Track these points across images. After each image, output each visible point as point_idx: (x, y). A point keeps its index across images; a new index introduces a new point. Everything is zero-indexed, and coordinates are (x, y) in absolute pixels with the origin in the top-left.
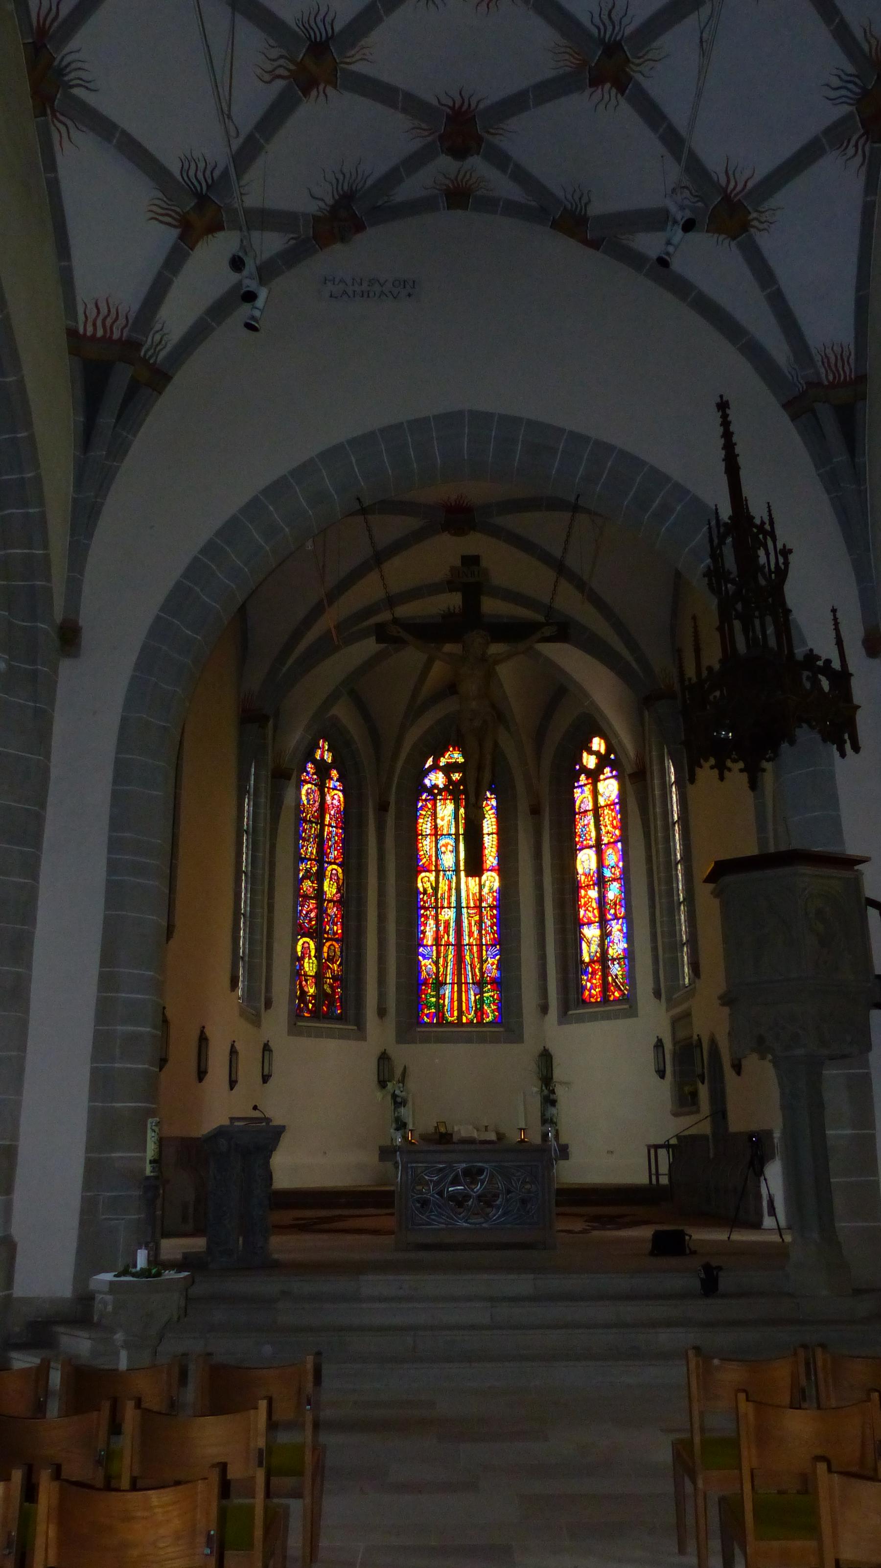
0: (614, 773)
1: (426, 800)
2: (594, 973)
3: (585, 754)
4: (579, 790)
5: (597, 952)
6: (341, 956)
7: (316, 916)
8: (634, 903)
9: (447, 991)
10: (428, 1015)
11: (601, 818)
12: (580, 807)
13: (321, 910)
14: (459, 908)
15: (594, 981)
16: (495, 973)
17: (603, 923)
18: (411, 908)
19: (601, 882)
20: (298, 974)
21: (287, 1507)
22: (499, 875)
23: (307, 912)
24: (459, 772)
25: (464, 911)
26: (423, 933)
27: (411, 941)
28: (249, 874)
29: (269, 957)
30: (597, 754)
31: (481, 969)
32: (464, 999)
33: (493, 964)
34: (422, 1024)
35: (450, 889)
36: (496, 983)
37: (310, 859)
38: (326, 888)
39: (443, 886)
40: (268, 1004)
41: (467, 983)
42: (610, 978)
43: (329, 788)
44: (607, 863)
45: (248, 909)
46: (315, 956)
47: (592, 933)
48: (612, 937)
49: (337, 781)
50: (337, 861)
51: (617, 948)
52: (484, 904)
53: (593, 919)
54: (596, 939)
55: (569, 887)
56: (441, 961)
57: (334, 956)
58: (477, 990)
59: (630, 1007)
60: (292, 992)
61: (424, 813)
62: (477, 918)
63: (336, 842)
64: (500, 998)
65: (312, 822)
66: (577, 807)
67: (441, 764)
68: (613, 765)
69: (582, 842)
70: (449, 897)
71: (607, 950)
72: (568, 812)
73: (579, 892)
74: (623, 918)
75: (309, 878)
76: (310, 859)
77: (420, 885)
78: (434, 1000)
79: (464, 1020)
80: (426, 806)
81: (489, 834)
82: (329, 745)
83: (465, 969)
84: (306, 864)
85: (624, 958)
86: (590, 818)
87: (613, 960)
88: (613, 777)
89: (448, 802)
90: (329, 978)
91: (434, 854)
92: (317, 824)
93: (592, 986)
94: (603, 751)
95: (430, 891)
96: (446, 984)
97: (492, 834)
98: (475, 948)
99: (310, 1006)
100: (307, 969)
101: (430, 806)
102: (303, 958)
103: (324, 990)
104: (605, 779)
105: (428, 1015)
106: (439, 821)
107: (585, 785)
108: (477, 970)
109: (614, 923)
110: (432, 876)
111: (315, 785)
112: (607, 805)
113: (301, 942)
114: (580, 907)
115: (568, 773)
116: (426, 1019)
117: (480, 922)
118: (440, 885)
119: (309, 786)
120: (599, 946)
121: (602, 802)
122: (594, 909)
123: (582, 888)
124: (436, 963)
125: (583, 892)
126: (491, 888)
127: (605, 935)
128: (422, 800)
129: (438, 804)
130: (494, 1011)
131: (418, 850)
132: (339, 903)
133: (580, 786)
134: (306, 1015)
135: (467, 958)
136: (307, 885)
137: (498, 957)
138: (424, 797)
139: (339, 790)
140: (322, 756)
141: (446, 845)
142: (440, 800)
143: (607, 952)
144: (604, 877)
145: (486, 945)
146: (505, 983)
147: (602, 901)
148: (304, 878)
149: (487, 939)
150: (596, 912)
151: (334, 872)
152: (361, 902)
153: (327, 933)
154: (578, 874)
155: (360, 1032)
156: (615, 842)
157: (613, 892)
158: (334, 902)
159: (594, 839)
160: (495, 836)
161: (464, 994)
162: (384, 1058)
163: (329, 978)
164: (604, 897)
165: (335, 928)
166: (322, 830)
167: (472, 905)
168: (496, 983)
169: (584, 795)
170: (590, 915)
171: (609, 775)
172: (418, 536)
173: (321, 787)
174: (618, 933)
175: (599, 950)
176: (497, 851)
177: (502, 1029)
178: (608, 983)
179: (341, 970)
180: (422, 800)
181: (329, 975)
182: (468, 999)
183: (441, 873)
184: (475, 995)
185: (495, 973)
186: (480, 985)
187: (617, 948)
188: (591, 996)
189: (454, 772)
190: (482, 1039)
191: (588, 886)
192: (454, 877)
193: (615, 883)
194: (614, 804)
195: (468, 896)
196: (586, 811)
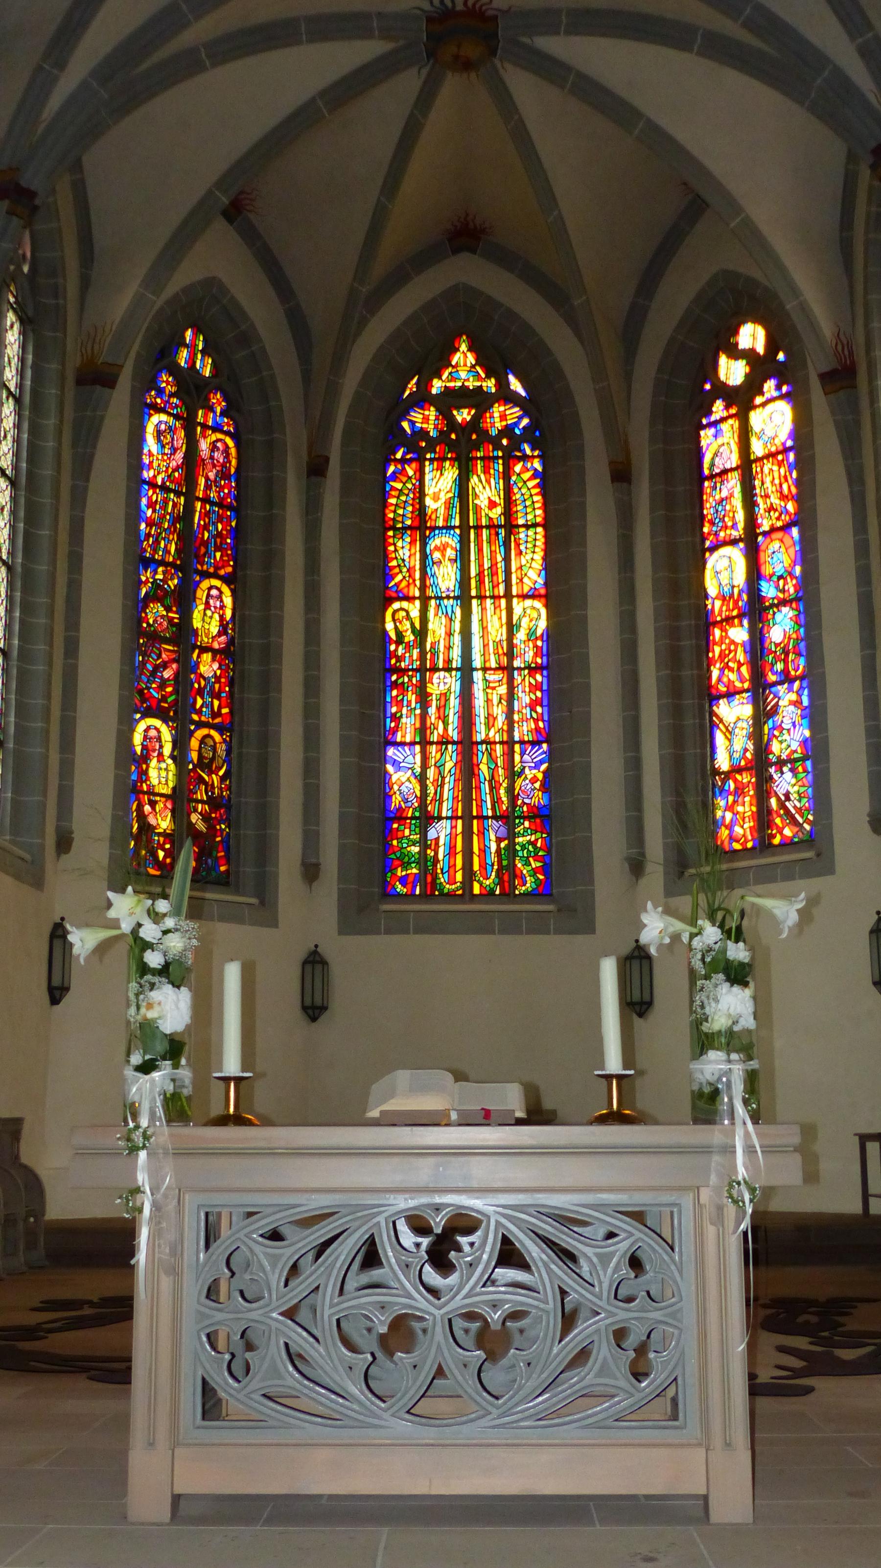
0: (785, 389)
1: (403, 461)
2: (740, 791)
3: (723, 359)
4: (711, 431)
5: (746, 750)
6: (228, 760)
7: (177, 675)
8: (830, 642)
9: (441, 831)
10: (403, 880)
11: (757, 483)
12: (712, 465)
13: (187, 668)
14: (466, 671)
15: (740, 809)
16: (538, 798)
17: (759, 688)
18: (376, 671)
19: (756, 610)
20: (133, 788)
21: (625, 1068)
22: (546, 606)
23: (156, 668)
24: (470, 407)
25: (478, 676)
26: (396, 718)
27: (371, 739)
28: (19, 569)
29: (67, 744)
30: (749, 355)
31: (510, 789)
32: (476, 849)
33: (534, 780)
34: (388, 894)
35: (449, 634)
36: (540, 817)
37: (162, 563)
38: (197, 623)
39: (436, 627)
40: (64, 843)
41: (481, 818)
42: (773, 802)
43: (205, 426)
44: (767, 570)
45: (16, 642)
46: (172, 757)
47: (735, 713)
48: (778, 718)
49: (223, 414)
50: (222, 572)
51: (790, 738)
52: (517, 663)
53: (738, 684)
54: (745, 725)
55: (689, 623)
56: (431, 773)
57: (213, 759)
58: (503, 832)
59: (818, 855)
60: (120, 821)
61: (399, 486)
62: (503, 690)
63: (219, 534)
64: (547, 848)
65: (167, 490)
66: (706, 465)
67: (434, 391)
68: (781, 374)
69: (716, 535)
70: (449, 648)
71: (768, 745)
72: (688, 476)
73: (708, 633)
74: (802, 678)
75: (159, 599)
76: (162, 563)
77: (389, 626)
78: (415, 849)
79: (477, 890)
80: (403, 472)
81: (527, 527)
82: (205, 340)
83: (478, 788)
84: (155, 572)
85: (804, 759)
86: (733, 485)
87: (780, 764)
88: (781, 397)
89: (447, 464)
90: (202, 802)
91: (418, 567)
92: (178, 494)
93: (735, 818)
94: (761, 349)
95: (409, 637)
96: (440, 818)
97: (535, 525)
98: (499, 749)
99: (161, 854)
100: (154, 781)
101: (410, 472)
102: (145, 758)
103: (191, 825)
104: (764, 405)
105: (403, 880)
106: (428, 501)
107: (723, 420)
108: (502, 791)
109: (782, 689)
110: (414, 609)
111: (177, 417)
112: (771, 455)
113: (141, 726)
114: (710, 662)
115: (690, 397)
116: (399, 888)
117: (511, 695)
118: (430, 626)
119: (163, 417)
120: (750, 737)
121: (758, 448)
122: (740, 665)
123: (715, 624)
124: (422, 779)
125: (717, 632)
126: (531, 633)
127: (763, 714)
128: (396, 461)
129: (427, 469)
130: (535, 871)
131: (386, 558)
132: (223, 654)
133: (714, 424)
134: (152, 871)
135: (483, 767)
136: (156, 612)
137: (544, 767)
138: (399, 455)
139: (227, 433)
140: (191, 361)
141: (442, 549)
142: (431, 460)
143: (767, 749)
144: (762, 599)
145: (522, 742)
146: (558, 816)
147: (757, 646)
148: (149, 599)
149: (524, 731)
150: (744, 670)
151: (214, 592)
152: (270, 654)
153: (199, 712)
154: (706, 597)
155: (265, 910)
156: (786, 528)
157: (782, 627)
158: (215, 652)
159: (741, 525)
160: (540, 530)
161: (475, 838)
162: (314, 962)
163: (202, 802)
164: (762, 640)
165: (216, 703)
166: (189, 509)
167: (493, 665)
168: (540, 817)
169: (720, 441)
170: (733, 676)
171: (776, 394)
172: (547, 21)
173: (189, 424)
174: (792, 708)
175: (750, 746)
176: (544, 559)
177: (551, 907)
178: (770, 811)
179: (229, 788)
180: (396, 461)
181: (201, 794)
182: (483, 851)
183: (433, 602)
184: (499, 840)
185: (538, 798)
186: (507, 819)
187: (790, 738)
188: (732, 838)
189: (458, 408)
190: (511, 926)
191: (729, 620)
192: (458, 611)
193: (785, 609)
194: (785, 450)
195: (485, 646)
196: (725, 472)
